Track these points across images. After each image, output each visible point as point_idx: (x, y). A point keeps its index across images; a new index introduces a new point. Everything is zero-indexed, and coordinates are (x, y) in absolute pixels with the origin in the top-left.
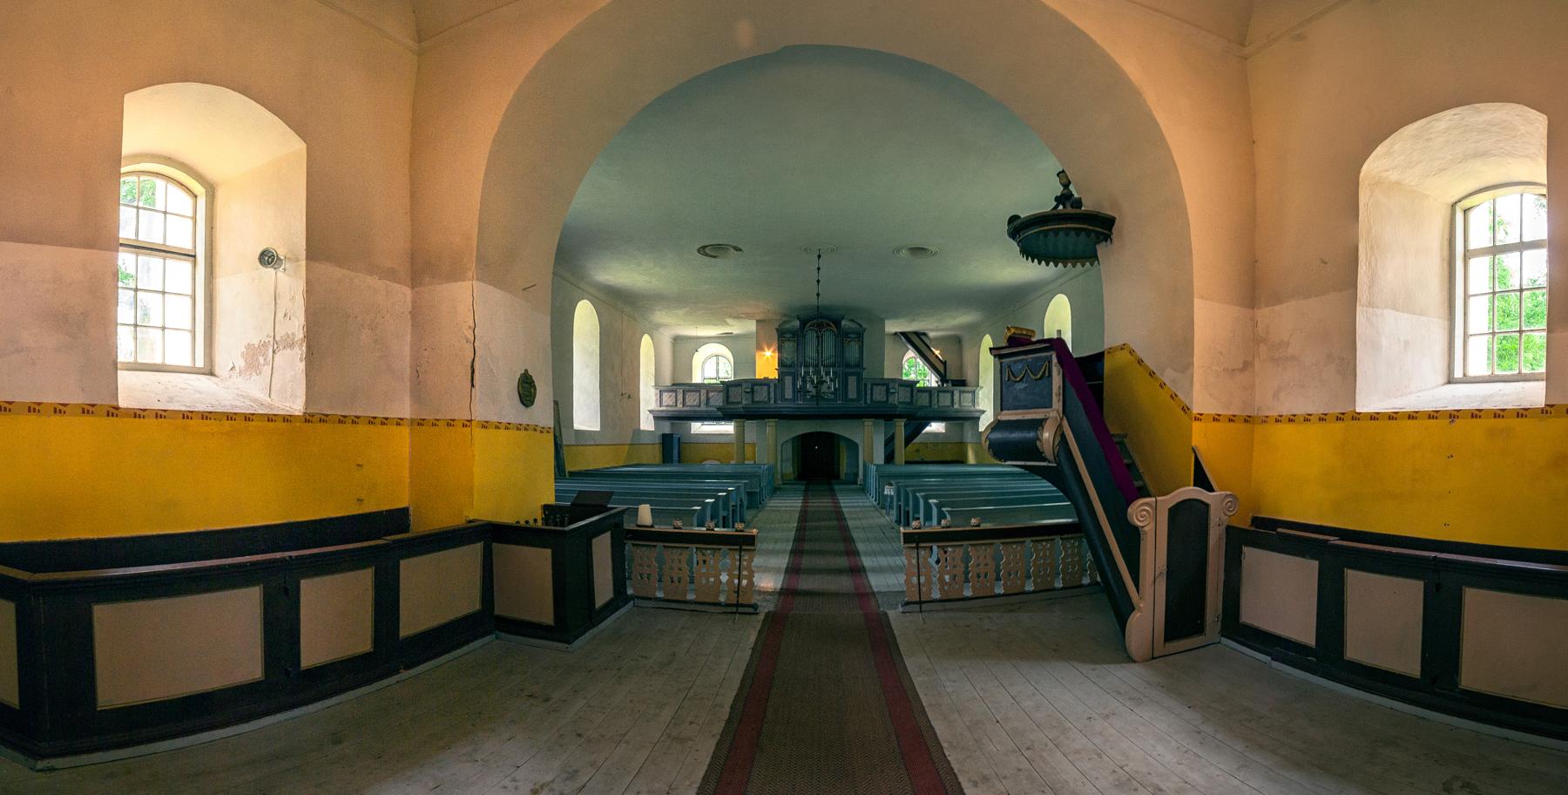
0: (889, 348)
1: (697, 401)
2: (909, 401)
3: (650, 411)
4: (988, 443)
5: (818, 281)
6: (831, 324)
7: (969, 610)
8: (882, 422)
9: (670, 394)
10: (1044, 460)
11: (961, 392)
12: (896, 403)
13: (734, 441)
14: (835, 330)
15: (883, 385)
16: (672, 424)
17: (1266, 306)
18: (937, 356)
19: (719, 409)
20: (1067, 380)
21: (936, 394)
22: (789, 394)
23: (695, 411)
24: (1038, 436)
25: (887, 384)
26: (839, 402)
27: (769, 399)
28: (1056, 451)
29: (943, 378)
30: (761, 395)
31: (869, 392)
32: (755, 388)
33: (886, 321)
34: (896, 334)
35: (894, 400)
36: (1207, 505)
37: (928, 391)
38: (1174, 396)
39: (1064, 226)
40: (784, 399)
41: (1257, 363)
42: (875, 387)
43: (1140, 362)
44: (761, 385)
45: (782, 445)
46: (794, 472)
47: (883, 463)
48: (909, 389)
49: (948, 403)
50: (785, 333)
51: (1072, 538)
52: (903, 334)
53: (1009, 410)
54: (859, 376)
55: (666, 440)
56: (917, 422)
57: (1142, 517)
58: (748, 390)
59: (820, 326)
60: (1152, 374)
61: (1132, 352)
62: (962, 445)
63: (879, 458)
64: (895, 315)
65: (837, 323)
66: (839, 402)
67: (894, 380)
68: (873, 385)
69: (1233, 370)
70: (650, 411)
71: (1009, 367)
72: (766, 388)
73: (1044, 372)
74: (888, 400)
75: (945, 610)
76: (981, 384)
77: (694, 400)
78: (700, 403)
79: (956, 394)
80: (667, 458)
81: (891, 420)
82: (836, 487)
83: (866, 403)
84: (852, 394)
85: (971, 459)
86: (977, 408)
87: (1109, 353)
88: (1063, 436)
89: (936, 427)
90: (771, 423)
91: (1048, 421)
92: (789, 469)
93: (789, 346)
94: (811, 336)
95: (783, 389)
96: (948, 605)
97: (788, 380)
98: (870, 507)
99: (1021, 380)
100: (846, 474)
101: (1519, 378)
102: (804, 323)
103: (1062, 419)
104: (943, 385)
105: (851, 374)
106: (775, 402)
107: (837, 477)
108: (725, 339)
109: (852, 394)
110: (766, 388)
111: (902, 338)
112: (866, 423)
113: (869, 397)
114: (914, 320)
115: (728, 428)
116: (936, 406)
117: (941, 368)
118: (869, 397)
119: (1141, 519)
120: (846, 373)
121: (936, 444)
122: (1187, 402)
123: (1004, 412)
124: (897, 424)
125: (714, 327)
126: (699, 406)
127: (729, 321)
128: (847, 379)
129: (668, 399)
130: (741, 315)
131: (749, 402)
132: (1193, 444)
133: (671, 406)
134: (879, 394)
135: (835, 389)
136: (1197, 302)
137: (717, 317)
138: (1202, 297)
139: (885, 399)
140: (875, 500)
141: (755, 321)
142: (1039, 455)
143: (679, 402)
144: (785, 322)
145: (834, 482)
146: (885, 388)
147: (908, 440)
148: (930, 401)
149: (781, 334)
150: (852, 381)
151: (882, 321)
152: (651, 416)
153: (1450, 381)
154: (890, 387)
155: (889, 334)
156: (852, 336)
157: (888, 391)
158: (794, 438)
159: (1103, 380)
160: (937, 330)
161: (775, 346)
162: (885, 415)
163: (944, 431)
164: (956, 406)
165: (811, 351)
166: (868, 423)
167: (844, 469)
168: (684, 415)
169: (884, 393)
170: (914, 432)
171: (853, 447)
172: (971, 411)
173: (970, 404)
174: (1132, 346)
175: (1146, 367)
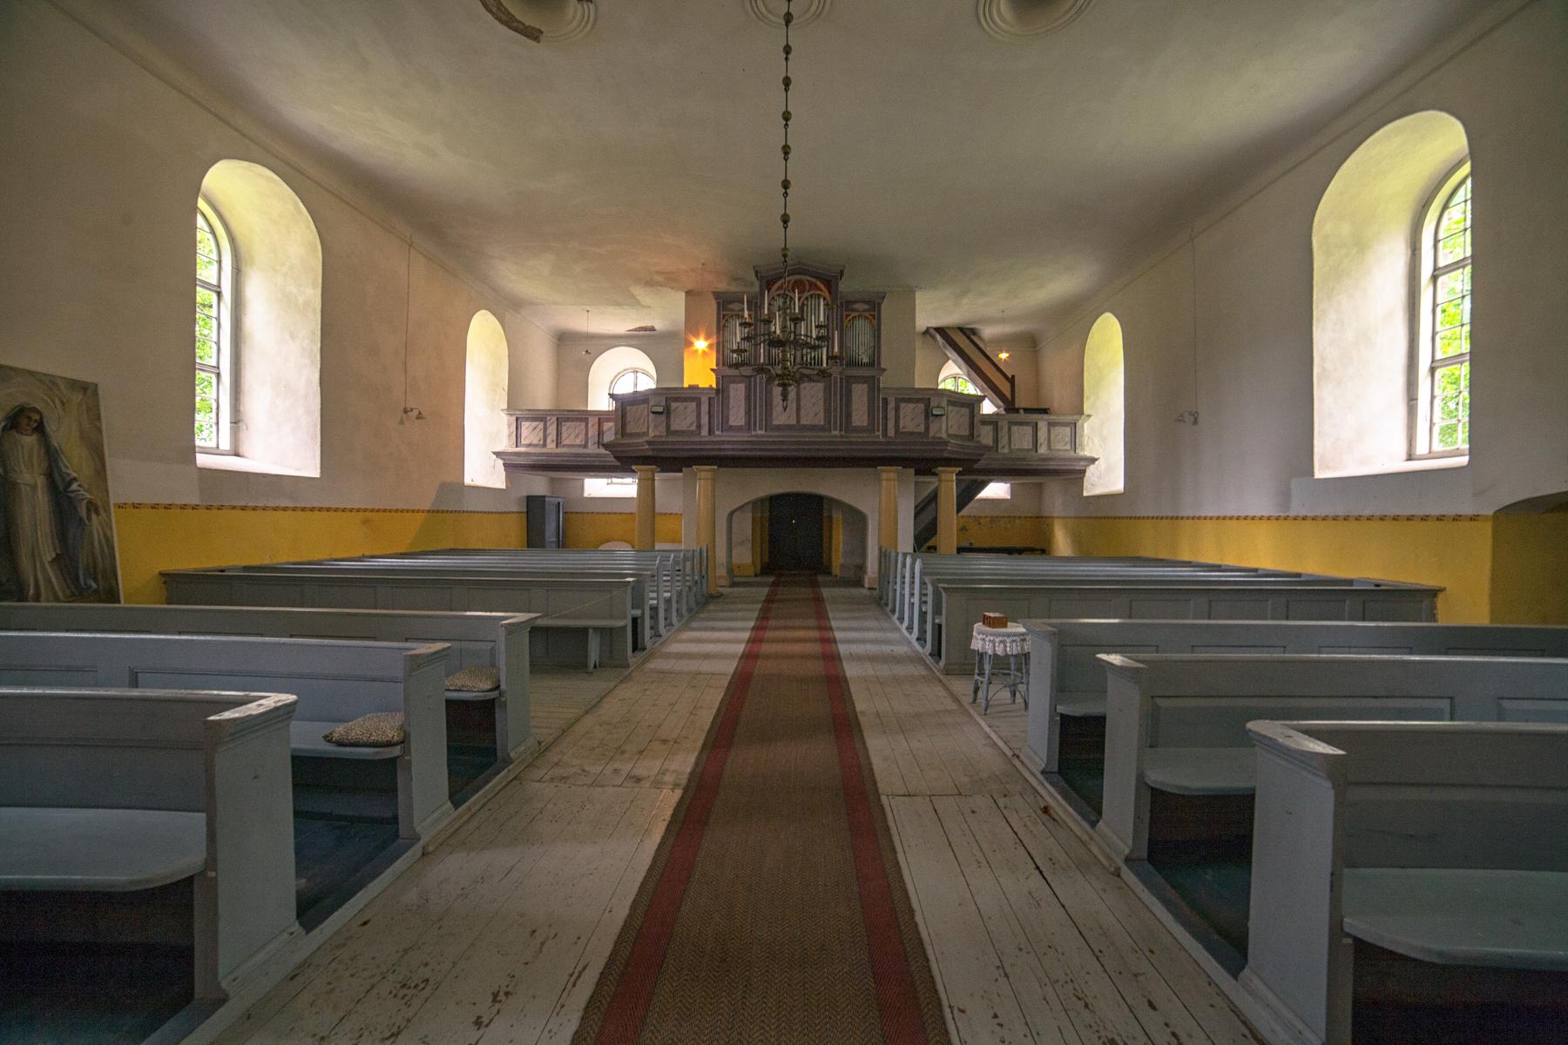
1: (582, 436)
2: (967, 433)
3: (498, 454)
6: (819, 283)
9: (534, 424)
11: (1051, 424)
12: (944, 436)
13: (634, 508)
15: (918, 401)
16: (552, 480)
21: (1006, 429)
22: (737, 417)
23: (577, 455)
26: (834, 433)
27: (699, 426)
29: (1010, 405)
30: (684, 419)
31: (891, 415)
33: (918, 295)
40: (726, 427)
42: (902, 405)
44: (685, 400)
46: (754, 563)
48: (965, 411)
49: (1027, 444)
52: (939, 330)
54: (873, 384)
55: (534, 506)
56: (974, 473)
58: (661, 409)
62: (1041, 524)
65: (830, 282)
66: (834, 433)
68: (899, 401)
70: (498, 454)
72: (694, 404)
74: (927, 429)
76: (1087, 410)
77: (577, 436)
78: (587, 442)
79: (1043, 427)
80: (534, 539)
81: (929, 472)
82: (826, 592)
85: (1062, 543)
86: (1081, 453)
89: (996, 490)
90: (704, 473)
92: (745, 556)
95: (725, 406)
97: (737, 392)
100: (843, 566)
101: (1431, 455)
102: (768, 282)
106: (710, 432)
109: (860, 417)
110: (694, 404)
111: (938, 337)
112: (884, 475)
113: (891, 424)
118: (891, 424)
120: (848, 378)
121: (994, 519)
126: (585, 446)
128: (849, 391)
129: (530, 433)
131: (662, 429)
133: (536, 446)
134: (911, 419)
139: (922, 429)
140: (910, 628)
141: (683, 294)
143: (549, 441)
145: (820, 578)
148: (996, 440)
149: (726, 304)
150: (860, 393)
152: (500, 462)
153: (1410, 458)
154: (932, 405)
157: (928, 413)
160: (1002, 321)
162: (924, 464)
163: (1009, 497)
164: (1043, 450)
166: (889, 474)
167: (839, 556)
168: (557, 461)
170: (967, 493)
171: (857, 520)
172: (1071, 459)
173: (1068, 447)
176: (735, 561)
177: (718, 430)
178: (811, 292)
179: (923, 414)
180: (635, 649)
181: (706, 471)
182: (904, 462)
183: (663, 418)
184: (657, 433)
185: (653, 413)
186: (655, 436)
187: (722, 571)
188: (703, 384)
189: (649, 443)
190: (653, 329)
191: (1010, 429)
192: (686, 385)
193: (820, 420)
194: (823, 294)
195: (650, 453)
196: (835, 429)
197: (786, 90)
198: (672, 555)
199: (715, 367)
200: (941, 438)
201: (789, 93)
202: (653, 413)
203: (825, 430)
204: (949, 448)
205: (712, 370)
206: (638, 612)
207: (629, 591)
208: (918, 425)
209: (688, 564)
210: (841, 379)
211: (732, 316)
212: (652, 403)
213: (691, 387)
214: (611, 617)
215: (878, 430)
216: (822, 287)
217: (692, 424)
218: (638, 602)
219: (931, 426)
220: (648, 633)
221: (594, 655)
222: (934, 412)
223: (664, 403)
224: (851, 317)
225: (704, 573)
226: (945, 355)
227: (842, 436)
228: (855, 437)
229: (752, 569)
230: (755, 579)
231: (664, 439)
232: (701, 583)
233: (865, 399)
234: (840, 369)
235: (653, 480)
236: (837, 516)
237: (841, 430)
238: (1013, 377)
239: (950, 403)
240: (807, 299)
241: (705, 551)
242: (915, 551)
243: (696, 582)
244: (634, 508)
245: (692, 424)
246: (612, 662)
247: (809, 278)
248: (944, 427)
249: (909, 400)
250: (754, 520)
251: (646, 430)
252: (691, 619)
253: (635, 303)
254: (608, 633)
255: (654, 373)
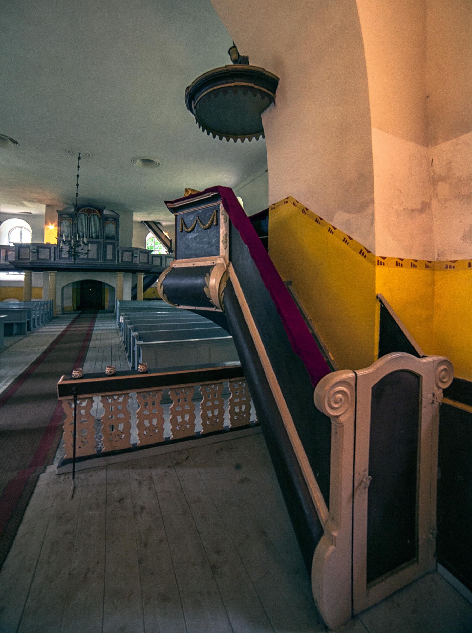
0: (136, 232)
2: (147, 262)
4: (162, 288)
5: (78, 176)
6: (96, 211)
7: (132, 465)
8: (130, 274)
10: (212, 305)
12: (138, 263)
14: (99, 215)
17: (447, 139)
18: (166, 236)
19: (11, 263)
20: (233, 226)
21: (164, 259)
24: (205, 282)
25: (132, 251)
27: (50, 257)
28: (222, 297)
29: (170, 250)
30: (44, 255)
31: (120, 255)
32: (40, 249)
33: (134, 213)
34: (142, 222)
35: (137, 261)
36: (418, 377)
37: (160, 256)
38: (347, 240)
39: (233, 84)
40: (61, 258)
41: (434, 203)
42: (124, 253)
43: (305, 211)
44: (45, 248)
45: (63, 289)
46: (73, 305)
47: (130, 300)
48: (146, 255)
50: (64, 214)
51: (240, 381)
52: (146, 222)
53: (182, 258)
57: (336, 403)
58: (35, 251)
59: (89, 212)
60: (318, 220)
61: (295, 203)
63: (127, 297)
64: (140, 209)
65: (101, 211)
67: (137, 249)
68: (123, 251)
69: (413, 210)
71: (182, 219)
72: (48, 250)
73: (212, 222)
74: (132, 260)
75: (106, 467)
83: (118, 262)
84: (109, 256)
87: (273, 208)
88: (229, 283)
91: (215, 267)
92: (69, 303)
93: (67, 223)
94: (83, 218)
96: (113, 459)
98: (114, 329)
99: (192, 230)
102: (78, 208)
103: (228, 266)
104: (170, 253)
105: (109, 244)
106: (55, 259)
107: (103, 308)
108: (26, 216)
110: (48, 250)
111: (145, 224)
112: (119, 275)
113: (120, 259)
114: (150, 214)
115: (20, 276)
116: (164, 266)
117: (169, 244)
118: (120, 259)
119: (336, 406)
122: (365, 244)
123: (178, 260)
124: (139, 276)
125: (15, 206)
127: (25, 203)
128: (106, 247)
130: (34, 200)
131: (35, 258)
132: (377, 292)
134: (127, 257)
135: (88, 251)
136: (375, 132)
137: (18, 201)
138: (380, 128)
139: (130, 260)
141: (45, 206)
142: (206, 301)
144: (67, 208)
146: (131, 253)
147: (146, 287)
148: (161, 263)
149: (61, 215)
151: (131, 213)
155: (138, 222)
156: (110, 219)
157: (133, 255)
158: (73, 283)
159: (267, 235)
161: (56, 223)
165: (82, 228)
166: (120, 275)
167: (107, 304)
169: (130, 257)
171: (112, 289)
174: (296, 198)
175: (312, 215)
176: (65, 305)
177: (57, 259)
178: (94, 213)
179: (131, 256)
180: (28, 330)
181: (53, 273)
182: (126, 271)
183: (36, 254)
184: (33, 259)
185: (32, 252)
186: (32, 260)
187: (59, 309)
188: (52, 243)
189: (29, 263)
190: (31, 213)
191: (166, 260)
192: (45, 242)
193: (95, 257)
194: (98, 214)
195: (30, 266)
196: (101, 260)
197: (78, 178)
198: (35, 303)
199: (57, 237)
200: (137, 263)
201: (79, 179)
202: (32, 252)
203: (97, 260)
204: (139, 267)
205: (56, 238)
206: (29, 320)
207: (26, 313)
208: (129, 259)
209: (45, 306)
210: (103, 244)
211: (64, 219)
212: (31, 248)
213: (48, 244)
214: (21, 320)
215: (116, 261)
216: (98, 212)
217: (47, 256)
218: (29, 317)
219: (134, 259)
220: (32, 325)
221: (15, 331)
222: (135, 255)
223: (36, 248)
224: (107, 223)
225: (51, 309)
226: (149, 231)
227: (103, 262)
228: (107, 263)
229: (72, 308)
230: (74, 312)
231: (36, 262)
232: (50, 312)
233: (112, 250)
234: (103, 240)
235: (31, 275)
236: (107, 288)
237: (103, 260)
238: (171, 240)
239: (140, 252)
240: (92, 215)
241: (52, 302)
242: (132, 300)
243: (48, 312)
244: (23, 285)
245: (47, 256)
246: (21, 333)
247: (93, 209)
248: (138, 260)
249: (126, 251)
250: (73, 289)
251: (28, 258)
252: (46, 324)
253: (24, 205)
254: (19, 325)
255: (31, 232)
